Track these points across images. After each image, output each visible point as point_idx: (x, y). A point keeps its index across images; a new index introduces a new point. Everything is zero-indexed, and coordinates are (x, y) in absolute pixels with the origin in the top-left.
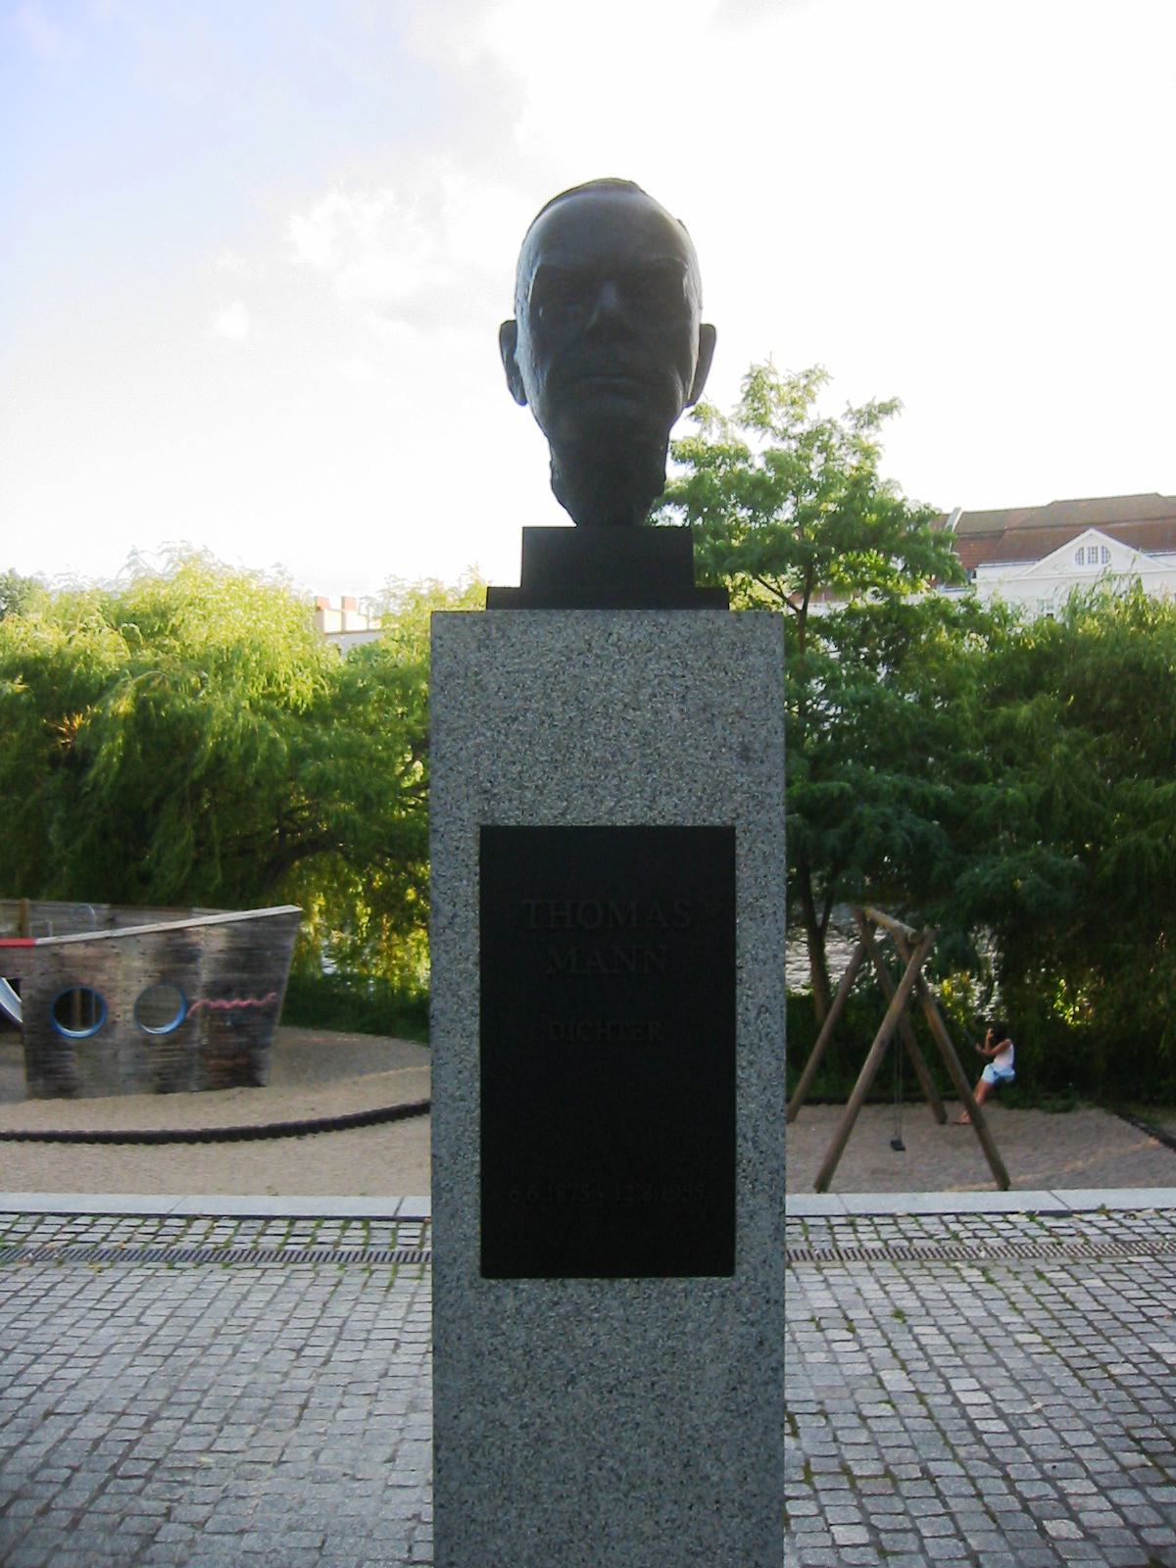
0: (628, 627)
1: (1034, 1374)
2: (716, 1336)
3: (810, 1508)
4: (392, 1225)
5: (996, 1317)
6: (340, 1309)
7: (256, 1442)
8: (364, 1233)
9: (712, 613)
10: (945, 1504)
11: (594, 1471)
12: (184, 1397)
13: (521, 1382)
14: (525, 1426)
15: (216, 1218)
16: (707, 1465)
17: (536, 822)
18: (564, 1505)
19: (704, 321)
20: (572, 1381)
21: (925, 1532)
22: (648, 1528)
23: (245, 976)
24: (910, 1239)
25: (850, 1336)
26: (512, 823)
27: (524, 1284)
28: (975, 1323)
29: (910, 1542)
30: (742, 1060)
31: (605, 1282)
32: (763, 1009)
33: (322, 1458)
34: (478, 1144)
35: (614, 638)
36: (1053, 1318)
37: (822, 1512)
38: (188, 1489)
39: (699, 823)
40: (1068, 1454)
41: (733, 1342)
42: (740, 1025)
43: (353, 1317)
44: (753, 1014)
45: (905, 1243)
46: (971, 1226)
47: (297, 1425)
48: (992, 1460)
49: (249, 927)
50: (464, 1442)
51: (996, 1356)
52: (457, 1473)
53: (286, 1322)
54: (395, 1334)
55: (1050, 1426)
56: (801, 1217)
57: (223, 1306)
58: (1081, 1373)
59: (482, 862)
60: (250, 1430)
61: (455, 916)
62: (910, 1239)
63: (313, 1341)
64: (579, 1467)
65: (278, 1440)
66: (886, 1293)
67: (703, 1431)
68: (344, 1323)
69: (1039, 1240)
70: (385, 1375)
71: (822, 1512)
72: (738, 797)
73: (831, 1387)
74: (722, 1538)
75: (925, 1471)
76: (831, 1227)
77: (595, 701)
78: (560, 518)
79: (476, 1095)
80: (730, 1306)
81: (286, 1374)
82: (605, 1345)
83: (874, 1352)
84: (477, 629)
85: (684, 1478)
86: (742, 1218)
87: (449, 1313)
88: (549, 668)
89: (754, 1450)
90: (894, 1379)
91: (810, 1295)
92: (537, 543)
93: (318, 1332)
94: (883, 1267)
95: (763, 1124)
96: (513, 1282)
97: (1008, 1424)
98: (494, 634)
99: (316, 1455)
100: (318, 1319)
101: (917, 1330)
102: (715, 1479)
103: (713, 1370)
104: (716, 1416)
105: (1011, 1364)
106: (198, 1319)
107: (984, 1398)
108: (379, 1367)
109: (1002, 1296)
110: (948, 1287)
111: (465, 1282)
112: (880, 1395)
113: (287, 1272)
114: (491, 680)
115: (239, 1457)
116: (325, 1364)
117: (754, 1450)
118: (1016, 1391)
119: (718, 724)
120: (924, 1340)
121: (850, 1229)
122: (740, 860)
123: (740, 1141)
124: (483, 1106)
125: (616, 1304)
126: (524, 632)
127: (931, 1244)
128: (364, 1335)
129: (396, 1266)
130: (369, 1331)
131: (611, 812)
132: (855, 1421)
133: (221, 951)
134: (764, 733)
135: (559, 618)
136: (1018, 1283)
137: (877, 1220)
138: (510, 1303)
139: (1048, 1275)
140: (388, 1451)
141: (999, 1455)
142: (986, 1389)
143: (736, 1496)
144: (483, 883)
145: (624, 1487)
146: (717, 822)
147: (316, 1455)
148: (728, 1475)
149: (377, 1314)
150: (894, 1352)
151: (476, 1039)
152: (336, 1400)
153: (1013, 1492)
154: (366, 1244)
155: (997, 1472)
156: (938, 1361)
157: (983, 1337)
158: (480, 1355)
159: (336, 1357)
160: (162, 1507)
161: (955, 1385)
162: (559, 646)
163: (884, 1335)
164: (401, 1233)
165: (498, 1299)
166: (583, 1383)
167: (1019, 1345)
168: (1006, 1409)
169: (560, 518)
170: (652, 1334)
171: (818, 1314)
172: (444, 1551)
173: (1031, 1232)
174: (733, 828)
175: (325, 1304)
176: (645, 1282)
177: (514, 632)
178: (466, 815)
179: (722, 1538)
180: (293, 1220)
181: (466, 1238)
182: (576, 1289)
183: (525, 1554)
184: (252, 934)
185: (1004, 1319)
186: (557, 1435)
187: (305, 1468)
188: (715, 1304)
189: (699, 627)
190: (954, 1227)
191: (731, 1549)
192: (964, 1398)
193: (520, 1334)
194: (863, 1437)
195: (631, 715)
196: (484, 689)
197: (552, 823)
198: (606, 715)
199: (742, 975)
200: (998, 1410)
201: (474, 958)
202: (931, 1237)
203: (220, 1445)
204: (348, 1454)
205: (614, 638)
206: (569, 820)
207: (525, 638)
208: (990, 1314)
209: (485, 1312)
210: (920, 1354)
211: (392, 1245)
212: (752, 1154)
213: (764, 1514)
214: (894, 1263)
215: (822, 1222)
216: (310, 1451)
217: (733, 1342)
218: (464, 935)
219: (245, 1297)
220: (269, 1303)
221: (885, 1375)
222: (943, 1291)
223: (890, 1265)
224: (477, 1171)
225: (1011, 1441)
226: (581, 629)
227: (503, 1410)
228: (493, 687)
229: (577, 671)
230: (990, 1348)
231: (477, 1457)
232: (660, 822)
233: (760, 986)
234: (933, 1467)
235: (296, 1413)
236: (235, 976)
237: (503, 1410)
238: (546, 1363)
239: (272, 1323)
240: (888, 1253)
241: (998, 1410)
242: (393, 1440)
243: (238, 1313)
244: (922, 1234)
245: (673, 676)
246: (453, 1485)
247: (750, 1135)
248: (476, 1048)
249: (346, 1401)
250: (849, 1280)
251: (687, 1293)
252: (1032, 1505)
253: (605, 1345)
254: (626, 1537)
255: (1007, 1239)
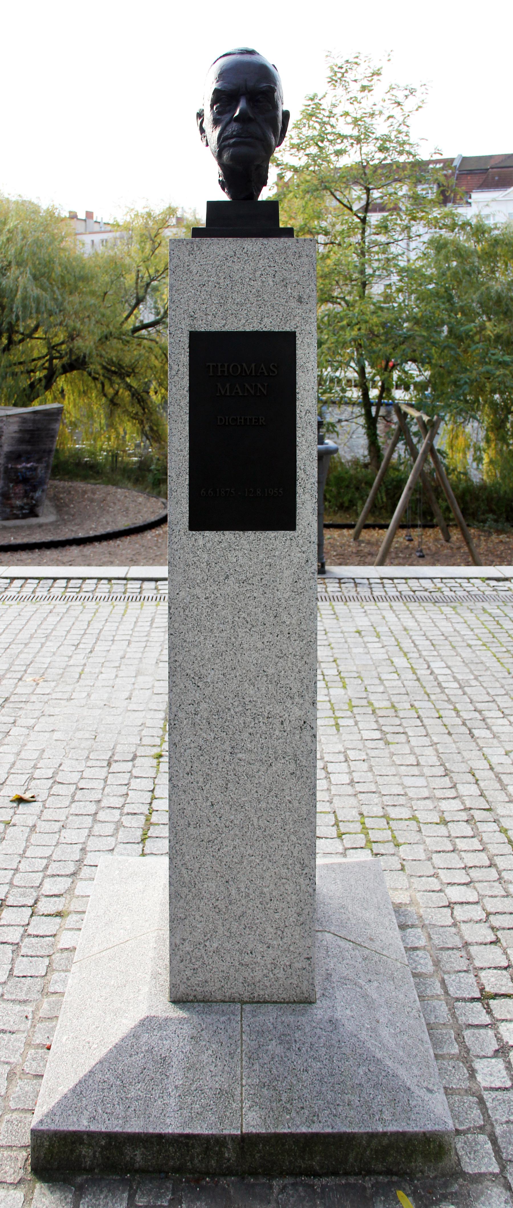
0: (252, 245)
1: (476, 660)
2: (288, 558)
3: (351, 722)
4: (124, 582)
5: (458, 632)
6: (97, 626)
7: (57, 690)
8: (109, 586)
9: (286, 239)
10: (422, 721)
11: (237, 619)
12: (17, 668)
13: (206, 578)
14: (206, 598)
15: (26, 579)
16: (285, 617)
17: (213, 329)
18: (224, 634)
19: (285, 109)
20: (227, 577)
21: (410, 734)
22: (259, 645)
23: (29, 448)
24: (414, 591)
25: (377, 640)
26: (203, 330)
27: (207, 533)
28: (446, 635)
29: (402, 738)
30: (299, 434)
31: (241, 532)
32: (308, 412)
33: (92, 698)
34: (188, 471)
35: (245, 250)
36: (490, 632)
37: (356, 723)
38: (24, 712)
39: (281, 330)
40: (491, 699)
41: (296, 561)
42: (298, 418)
43: (105, 628)
44: (303, 414)
45: (412, 593)
46: (449, 585)
47: (78, 682)
48: (449, 701)
49: (32, 417)
50: (182, 605)
51: (456, 652)
52: (178, 619)
53: (68, 632)
54: (128, 638)
55: (482, 685)
56: (353, 579)
57: (33, 625)
58: (502, 661)
59: (190, 347)
60: (54, 684)
61: (178, 370)
62: (414, 591)
63: (83, 641)
64: (230, 617)
65: (69, 688)
66: (399, 619)
67: (283, 601)
68: (100, 632)
69: (486, 593)
70: (123, 658)
71: (356, 723)
72: (297, 319)
73: (364, 665)
74: (291, 650)
75: (412, 706)
76: (370, 584)
77: (237, 278)
78: (223, 196)
79: (187, 449)
80: (294, 544)
81: (71, 657)
82: (241, 561)
83: (390, 648)
84: (189, 247)
85: (275, 622)
86: (299, 505)
87: (175, 547)
88: (218, 263)
89: (305, 610)
90: (400, 662)
91: (356, 619)
92: (214, 208)
93: (86, 636)
94: (398, 606)
95: (308, 462)
96: (202, 533)
97: (459, 684)
98: (195, 249)
99: (89, 695)
100: (86, 630)
101: (413, 638)
102: (288, 623)
103: (287, 573)
104: (288, 594)
105: (464, 655)
106: (21, 630)
107: (448, 671)
108: (121, 653)
109: (462, 621)
110: (433, 616)
111: (182, 533)
112: (392, 669)
113: (67, 606)
114: (194, 268)
115: (50, 696)
116: (91, 652)
117: (305, 610)
118: (465, 668)
119: (289, 286)
120: (417, 643)
121: (381, 586)
122: (298, 346)
123: (298, 470)
124: (190, 454)
125: (245, 543)
126: (208, 248)
127: (427, 594)
128: (112, 638)
129: (127, 603)
130: (114, 636)
131: (244, 325)
132: (377, 682)
133: (15, 432)
134: (308, 291)
135: (223, 241)
136: (473, 615)
137: (396, 581)
138: (201, 542)
139: (490, 611)
140: (127, 694)
141: (453, 699)
142: (448, 667)
143: (297, 631)
144: (190, 356)
145: (249, 626)
146: (288, 330)
147: (89, 695)
148: (294, 622)
149: (118, 627)
150: (400, 648)
151: (187, 424)
152: (97, 670)
153: (458, 716)
154: (109, 592)
155: (451, 707)
156: (424, 653)
157: (450, 642)
158: (188, 565)
159: (96, 648)
160: (12, 720)
161: (432, 665)
162: (222, 253)
163: (396, 640)
164: (129, 586)
165: (196, 540)
166: (232, 578)
167: (469, 646)
168: (459, 677)
169: (223, 196)
170: (261, 557)
171: (360, 629)
172: (172, 655)
173: (482, 589)
174: (295, 332)
175: (89, 622)
176: (258, 533)
177: (204, 248)
178: (183, 327)
179: (291, 650)
180: (69, 579)
181: (182, 513)
182: (229, 535)
183: (207, 657)
184: (34, 421)
185: (462, 633)
186: (221, 602)
187: (83, 702)
188: (288, 542)
189: (280, 246)
190: (440, 585)
191: (295, 656)
192: (436, 671)
193: (205, 556)
194: (381, 689)
195: (252, 283)
196: (191, 272)
197: (219, 330)
198: (242, 283)
199: (298, 396)
200: (454, 677)
201: (187, 389)
202: (426, 590)
203: (38, 691)
204: (106, 695)
205: (245, 250)
206: (226, 329)
207: (208, 250)
208: (455, 630)
209: (191, 546)
210: (415, 650)
211: (125, 593)
212: (303, 476)
213: (309, 639)
214: (405, 604)
215: (366, 581)
216: (86, 694)
217: (296, 561)
218: (183, 378)
219: (45, 619)
220: (59, 622)
221: (395, 660)
222: (430, 618)
223: (402, 604)
224: (187, 482)
225: (460, 692)
226: (231, 246)
227: (198, 591)
228: (195, 271)
229: (230, 264)
230: (454, 648)
231: (187, 612)
232: (265, 329)
233: (306, 401)
234: (416, 704)
235: (78, 676)
236: (24, 447)
237: (198, 591)
238: (216, 570)
239: (61, 631)
240: (401, 597)
241: (454, 677)
242: (130, 689)
243: (43, 627)
244: (421, 589)
245: (270, 266)
246: (176, 625)
247: (302, 467)
248: (187, 428)
249: (103, 670)
250: (379, 612)
251: (276, 538)
252: (467, 722)
253: (241, 561)
254: (250, 649)
255: (468, 592)
